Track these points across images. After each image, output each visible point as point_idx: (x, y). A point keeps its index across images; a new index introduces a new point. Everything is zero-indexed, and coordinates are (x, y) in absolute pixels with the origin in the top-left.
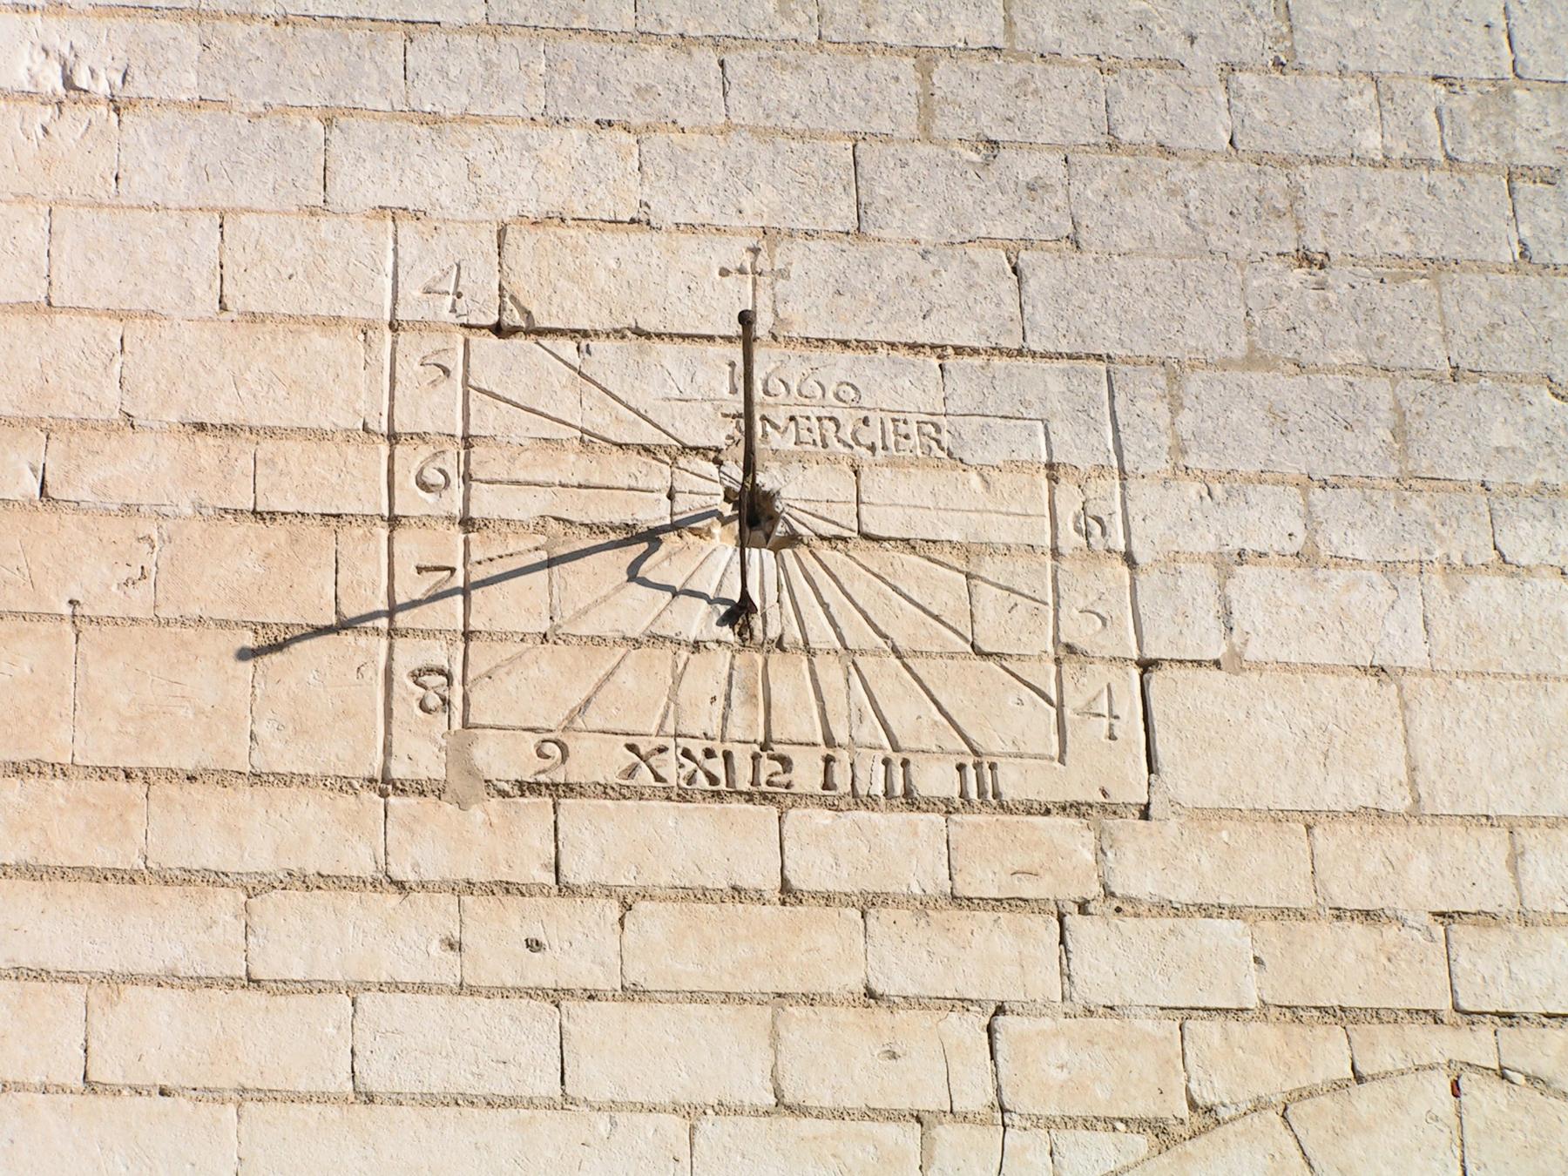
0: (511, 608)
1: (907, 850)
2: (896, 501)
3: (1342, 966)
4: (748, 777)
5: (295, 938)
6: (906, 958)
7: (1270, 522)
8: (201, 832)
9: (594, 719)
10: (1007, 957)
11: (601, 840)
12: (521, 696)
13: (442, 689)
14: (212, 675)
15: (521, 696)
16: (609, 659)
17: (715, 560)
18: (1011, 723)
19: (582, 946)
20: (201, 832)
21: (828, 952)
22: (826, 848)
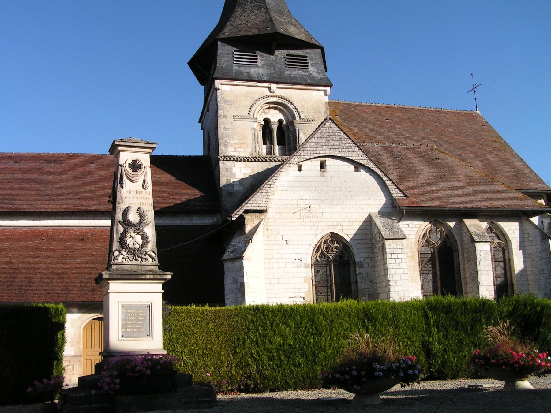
0: (302, 211)
1: (314, 220)
2: (315, 206)
3: (329, 224)
4: (310, 217)
5: (296, 224)
6: (315, 224)
7: (327, 206)
8: (293, 220)
9: (227, 33)
10: (318, 224)
11: (305, 220)
12: (302, 215)
13: (300, 215)
14: (292, 214)
15: (302, 215)
16: (305, 213)
17: (308, 209)
18: (318, 215)
19: (304, 224)
20: (293, 220)
21: (312, 224)
22: (313, 220)
